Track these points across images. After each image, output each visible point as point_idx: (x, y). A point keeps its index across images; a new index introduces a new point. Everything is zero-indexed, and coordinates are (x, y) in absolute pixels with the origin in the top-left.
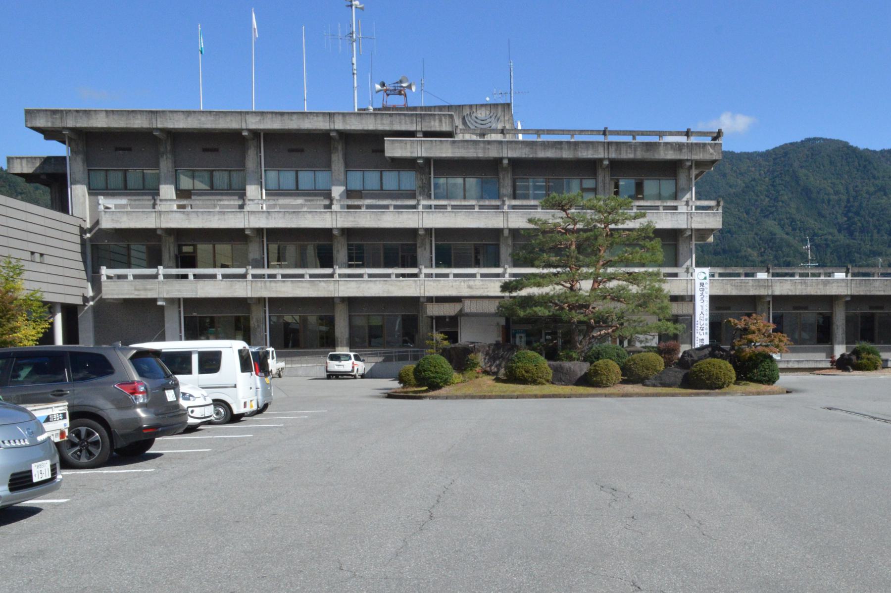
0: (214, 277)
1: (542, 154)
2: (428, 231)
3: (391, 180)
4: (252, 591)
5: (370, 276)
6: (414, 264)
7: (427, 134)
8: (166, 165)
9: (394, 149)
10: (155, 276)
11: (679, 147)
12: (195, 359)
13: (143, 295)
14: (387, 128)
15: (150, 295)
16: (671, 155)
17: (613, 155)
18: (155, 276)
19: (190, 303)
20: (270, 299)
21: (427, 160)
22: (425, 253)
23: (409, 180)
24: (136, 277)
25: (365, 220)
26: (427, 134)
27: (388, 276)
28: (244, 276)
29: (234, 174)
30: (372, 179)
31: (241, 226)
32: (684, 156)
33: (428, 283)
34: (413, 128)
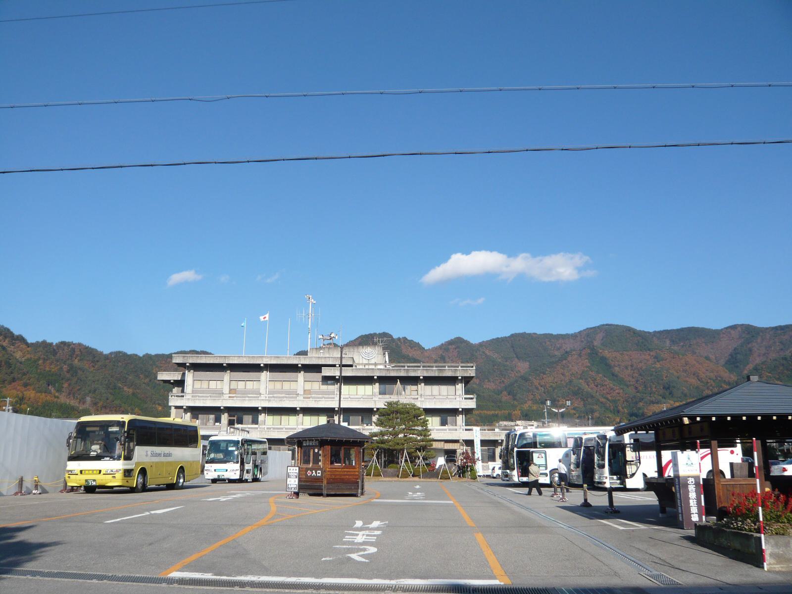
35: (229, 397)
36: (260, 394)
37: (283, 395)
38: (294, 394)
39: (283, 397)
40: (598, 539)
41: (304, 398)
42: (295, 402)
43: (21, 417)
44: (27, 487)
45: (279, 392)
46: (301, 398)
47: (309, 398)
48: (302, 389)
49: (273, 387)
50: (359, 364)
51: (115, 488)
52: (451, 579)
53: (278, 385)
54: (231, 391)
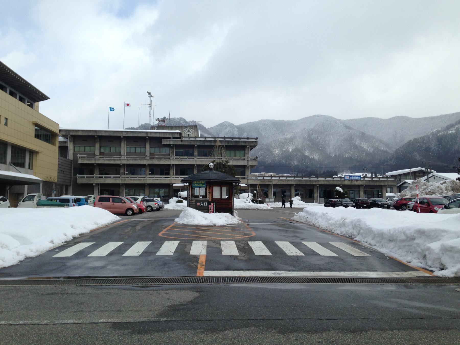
0: (111, 177)
1: (206, 144)
2: (173, 165)
3: (163, 150)
4: (73, 343)
5: (156, 177)
6: (168, 174)
7: (174, 138)
8: (97, 145)
9: (165, 142)
10: (93, 177)
11: (245, 142)
12: (111, 199)
13: (89, 183)
14: (163, 136)
15: (91, 183)
16: (243, 144)
17: (227, 144)
18: (93, 177)
19: (102, 185)
20: (126, 184)
21: (174, 145)
22: (172, 172)
23: (167, 150)
24: (87, 177)
25: (155, 162)
26: (174, 138)
27: (162, 177)
28: (119, 177)
29: (117, 148)
30: (157, 150)
31: (145, 163)
32: (247, 144)
33: (196, 160)
34: (170, 136)
35: (100, 157)
36: (121, 156)
37: (137, 156)
38: (143, 155)
39: (137, 158)
40: (9, 286)
41: (150, 158)
42: (145, 161)
43: (34, 132)
44: (457, 179)
45: (133, 155)
46: (148, 158)
47: (154, 158)
48: (149, 153)
49: (129, 151)
50: (185, 137)
51: (198, 228)
52: (331, 271)
53: (133, 150)
54: (101, 153)
